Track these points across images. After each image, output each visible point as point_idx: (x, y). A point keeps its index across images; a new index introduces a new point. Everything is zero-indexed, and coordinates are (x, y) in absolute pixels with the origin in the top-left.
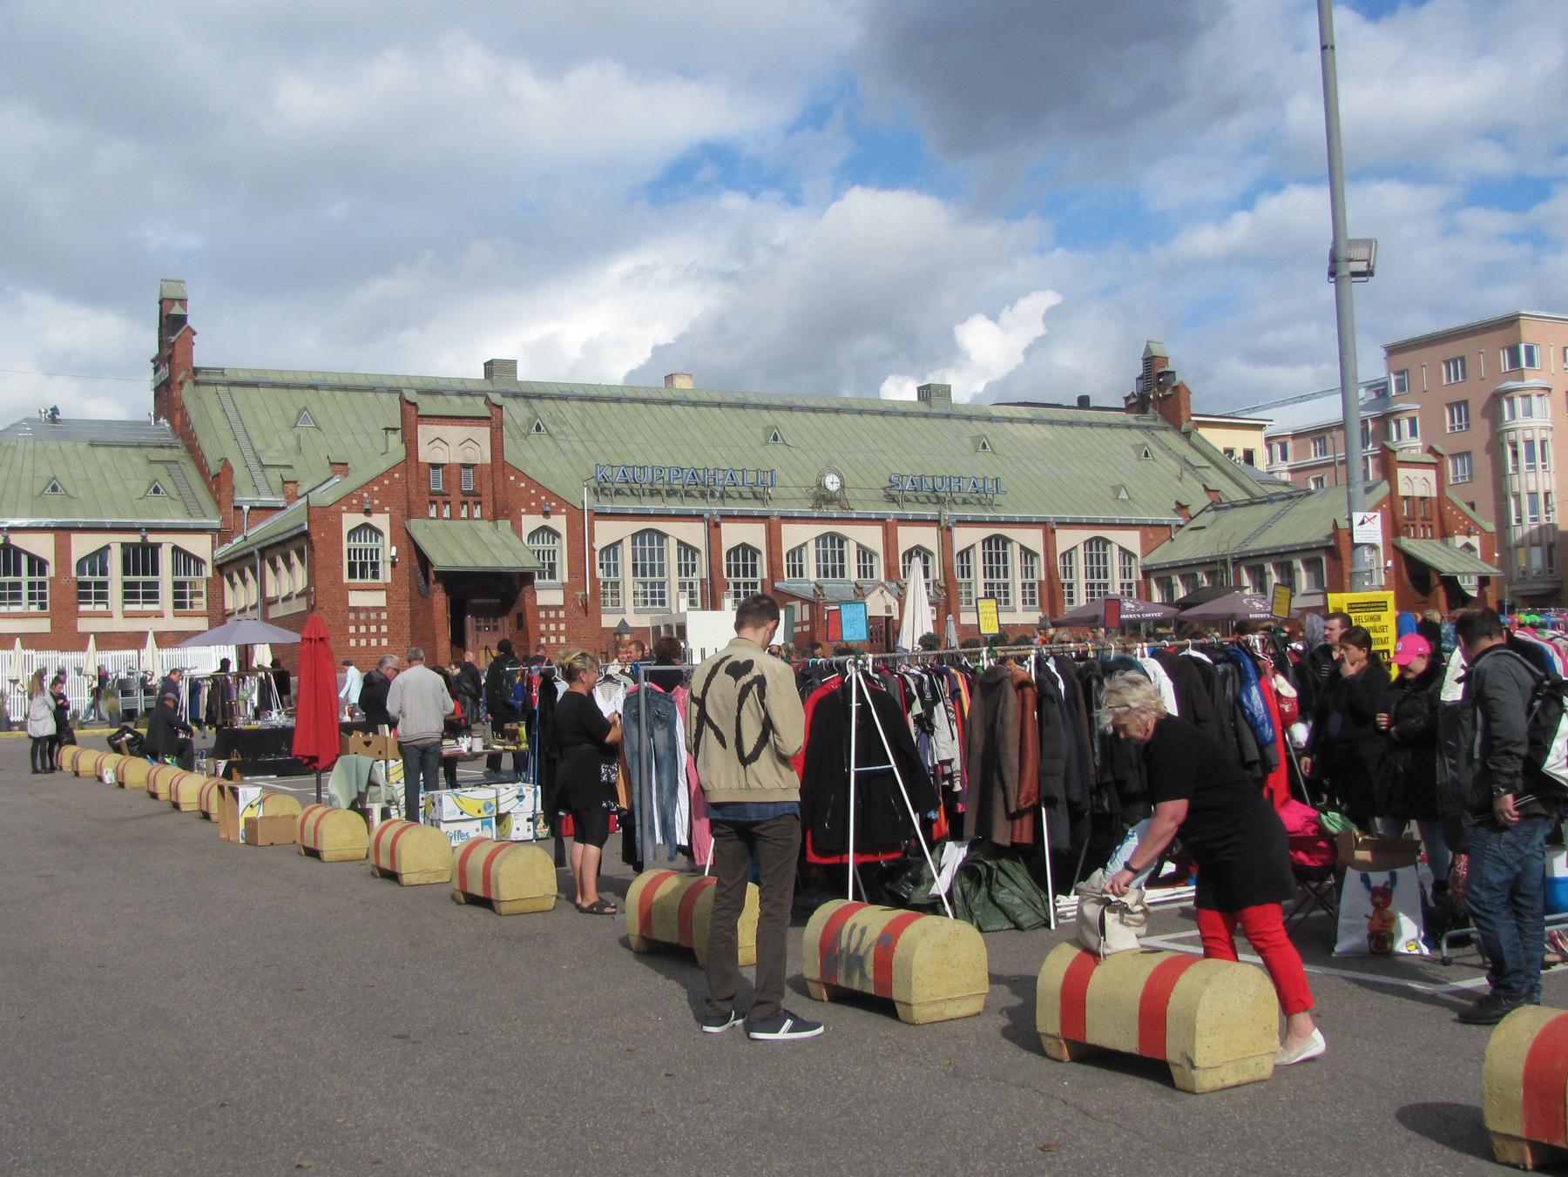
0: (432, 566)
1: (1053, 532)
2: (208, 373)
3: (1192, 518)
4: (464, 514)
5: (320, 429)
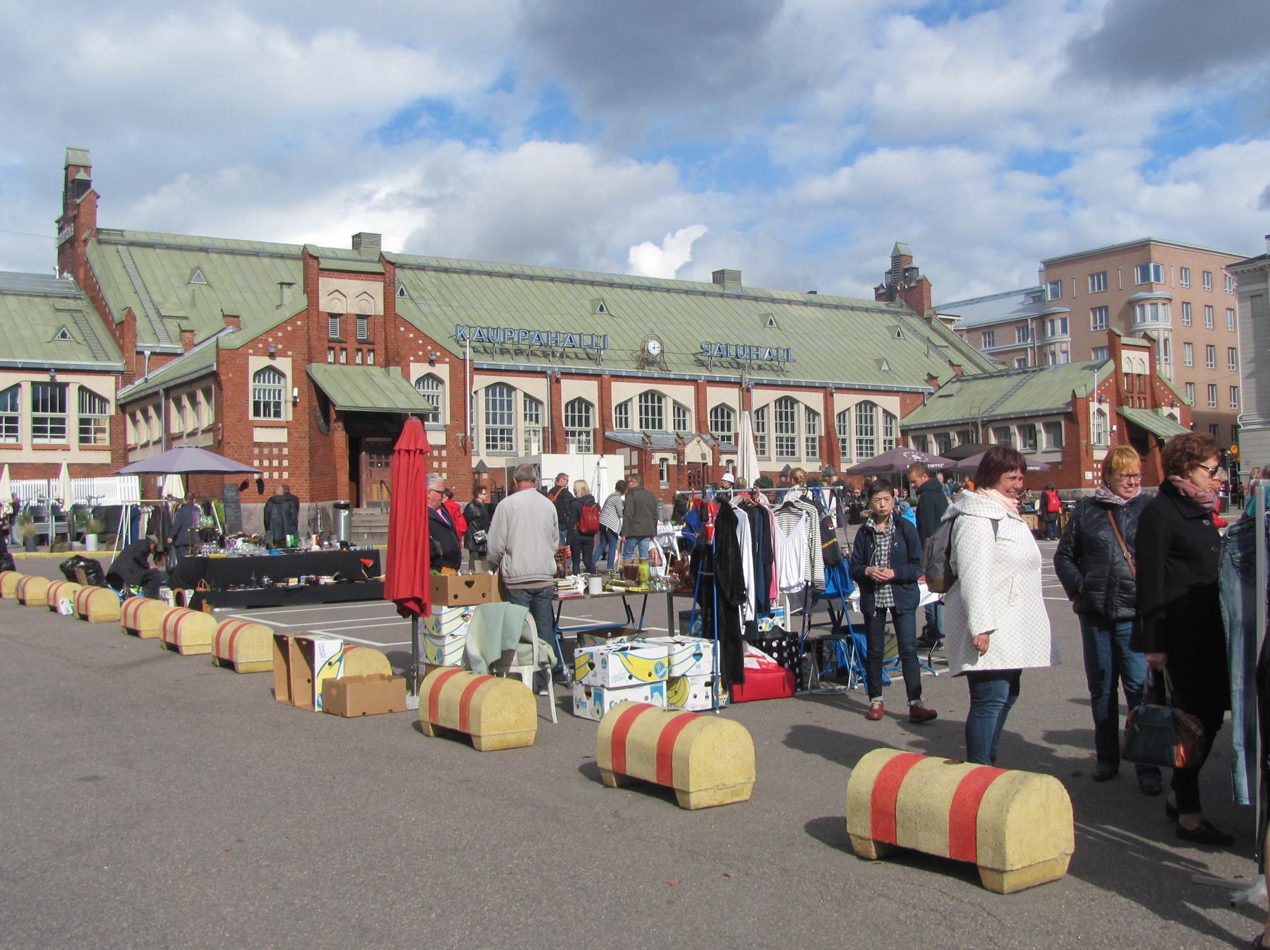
0: (334, 406)
1: (832, 395)
2: (108, 234)
3: (940, 388)
4: (358, 360)
5: (211, 287)
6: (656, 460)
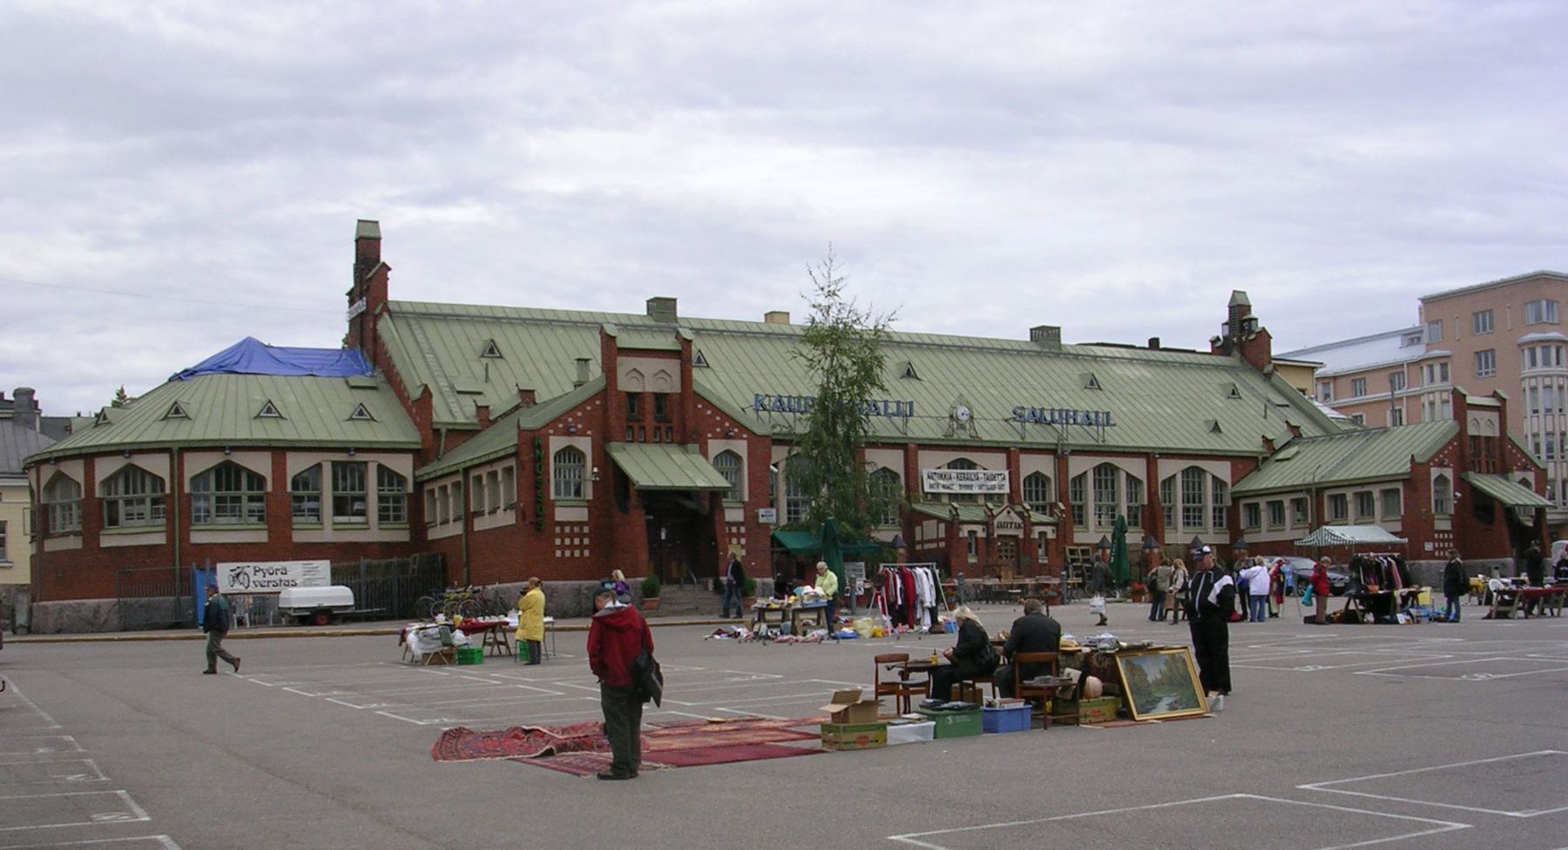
6: (964, 532)
